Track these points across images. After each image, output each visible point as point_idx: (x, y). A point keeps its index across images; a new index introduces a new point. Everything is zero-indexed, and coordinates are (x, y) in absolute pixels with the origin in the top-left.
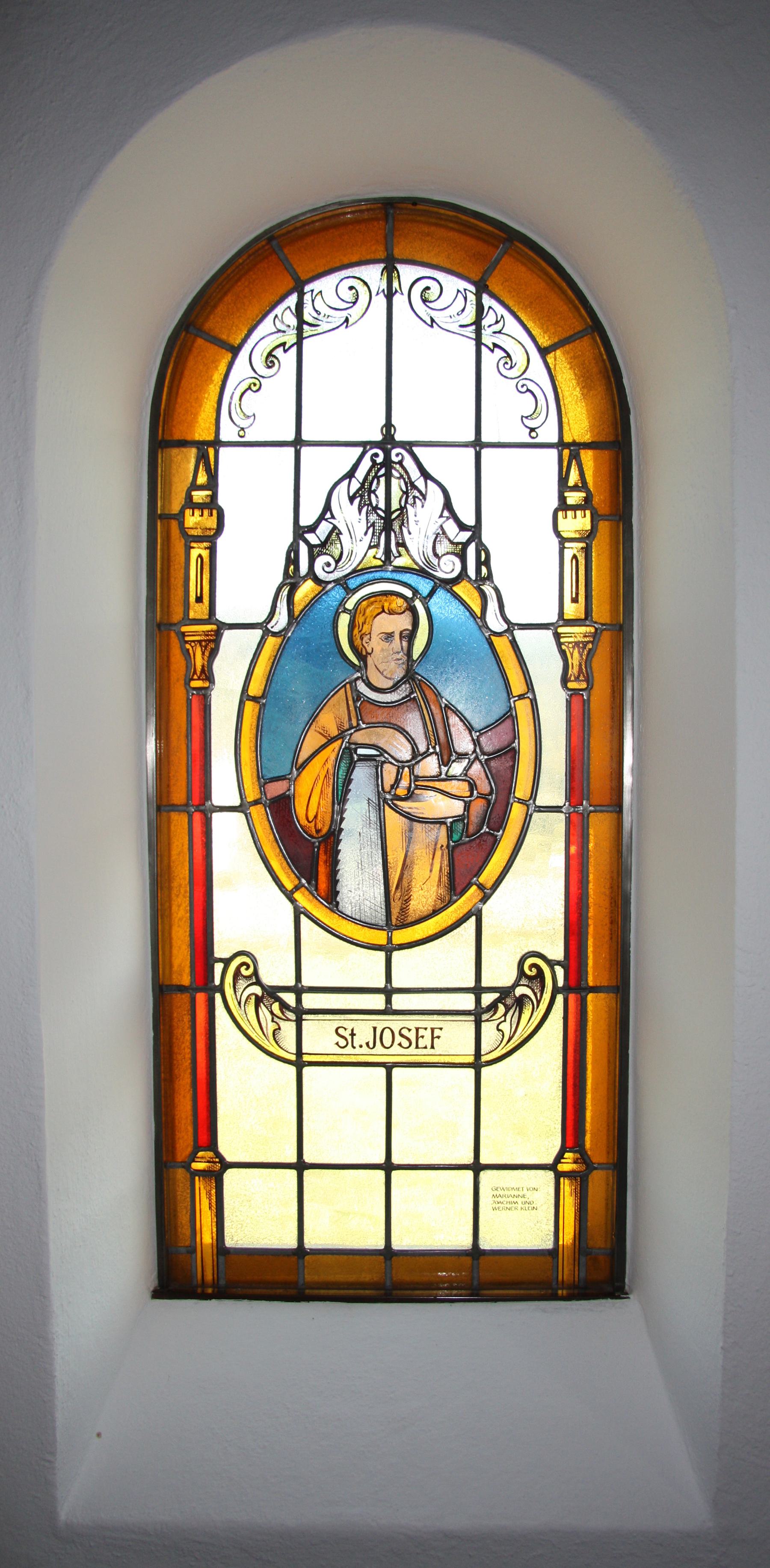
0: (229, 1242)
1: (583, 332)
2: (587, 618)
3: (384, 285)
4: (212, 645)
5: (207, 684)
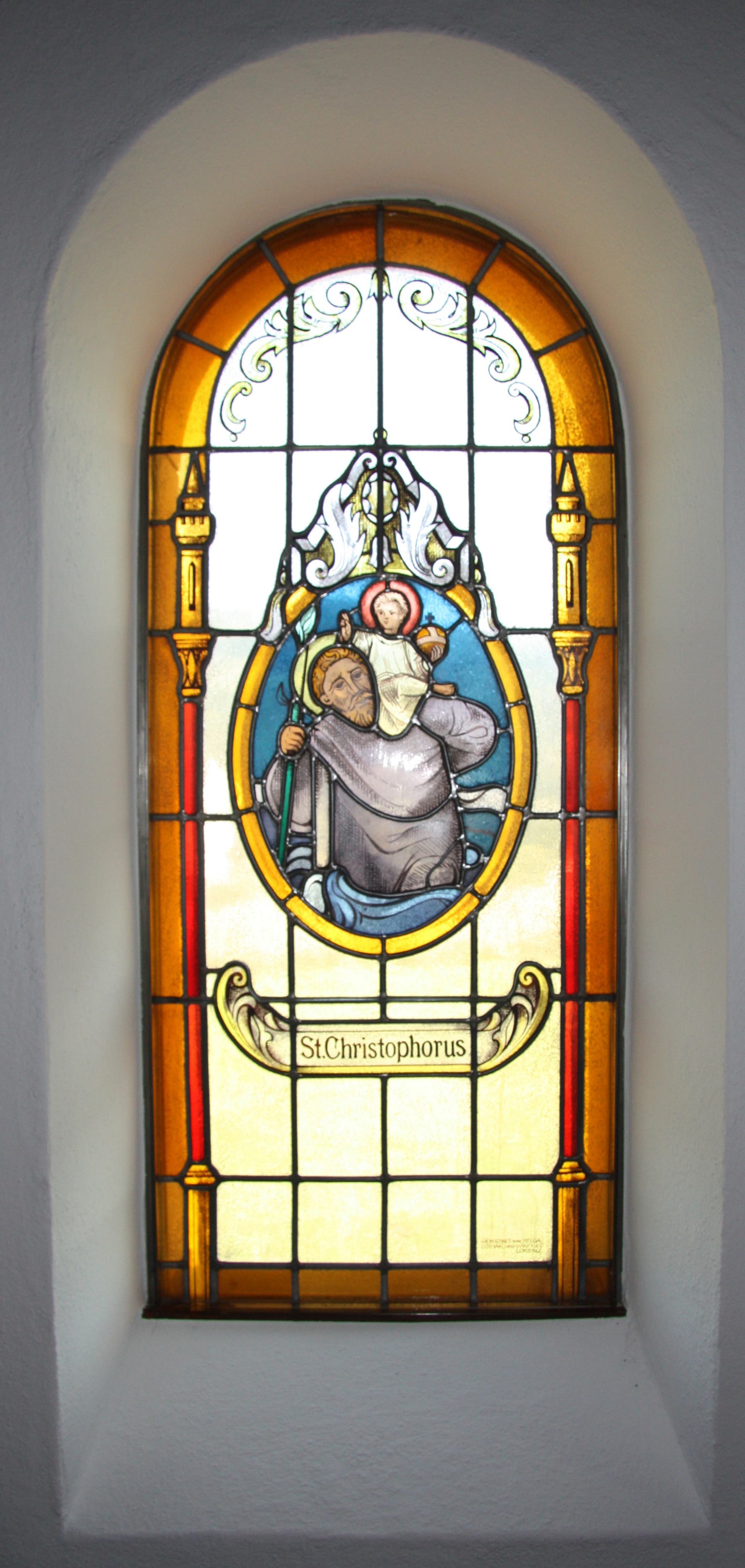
0: (222, 1257)
1: (575, 332)
2: (581, 623)
3: (375, 290)
4: (203, 655)
5: (197, 691)
